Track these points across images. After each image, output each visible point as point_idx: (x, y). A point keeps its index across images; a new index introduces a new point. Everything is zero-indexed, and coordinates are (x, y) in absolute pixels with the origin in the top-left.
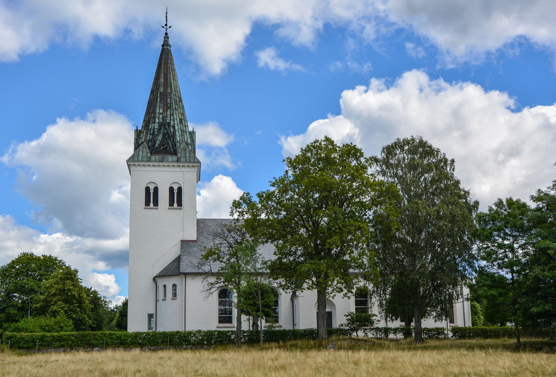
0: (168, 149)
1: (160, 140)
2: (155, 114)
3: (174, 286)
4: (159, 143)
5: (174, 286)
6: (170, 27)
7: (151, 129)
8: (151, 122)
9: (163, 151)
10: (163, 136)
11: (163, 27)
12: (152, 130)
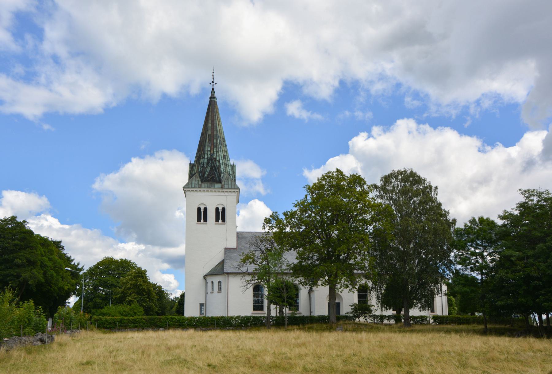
3: (220, 282)
5: (220, 282)
6: (216, 84)
11: (211, 84)
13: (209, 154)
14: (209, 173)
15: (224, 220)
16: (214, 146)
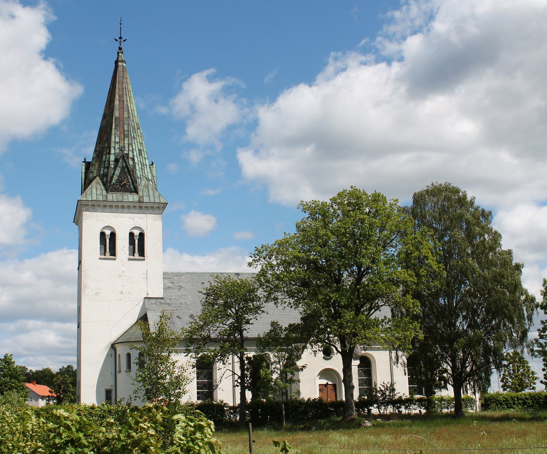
0: (127, 186)
1: (118, 175)
2: (110, 143)
4: (117, 178)
7: (105, 162)
8: (105, 153)
9: (121, 188)
10: (121, 169)
11: (116, 40)
12: (106, 162)
13: (116, 148)
14: (119, 177)
15: (142, 253)
16: (124, 135)
